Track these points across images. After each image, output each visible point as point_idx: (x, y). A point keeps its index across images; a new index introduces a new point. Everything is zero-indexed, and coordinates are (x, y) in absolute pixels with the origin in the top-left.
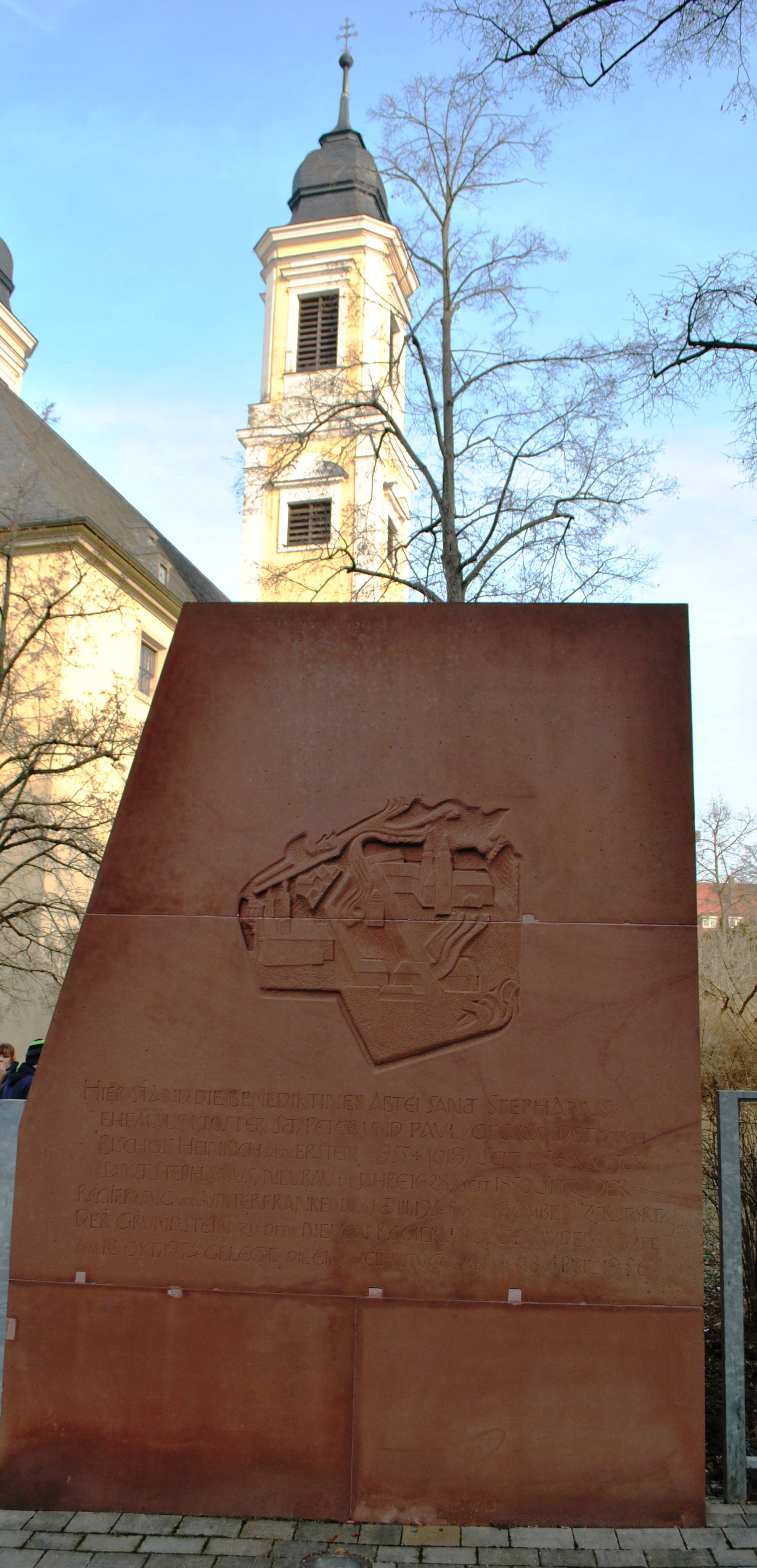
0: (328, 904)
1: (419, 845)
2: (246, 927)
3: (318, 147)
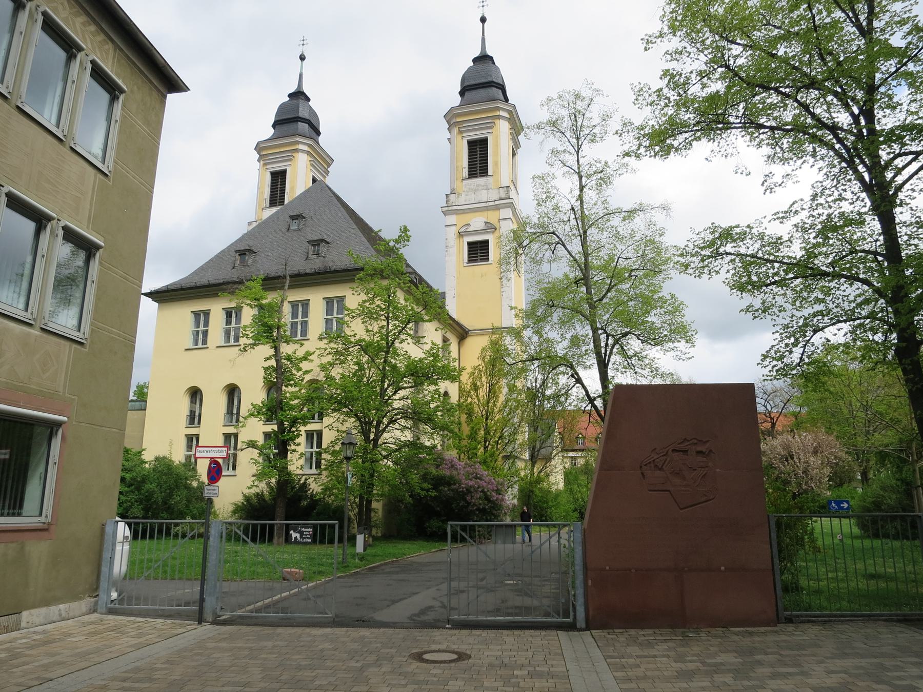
0: (664, 467)
1: (687, 451)
2: (642, 474)
3: (472, 64)
